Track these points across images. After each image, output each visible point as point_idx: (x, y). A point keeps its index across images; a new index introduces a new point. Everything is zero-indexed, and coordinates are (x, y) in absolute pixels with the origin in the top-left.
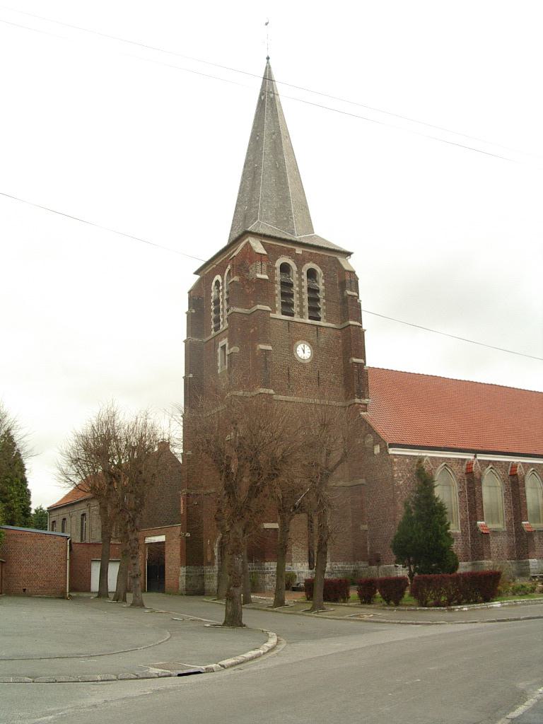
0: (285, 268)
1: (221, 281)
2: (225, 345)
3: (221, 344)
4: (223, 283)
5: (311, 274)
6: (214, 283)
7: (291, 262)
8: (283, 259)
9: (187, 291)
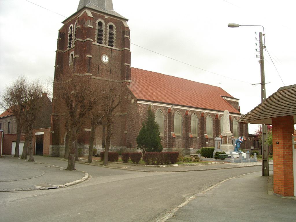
0: (100, 24)
1: (73, 27)
2: (73, 54)
3: (71, 53)
5: (111, 27)
6: (70, 28)
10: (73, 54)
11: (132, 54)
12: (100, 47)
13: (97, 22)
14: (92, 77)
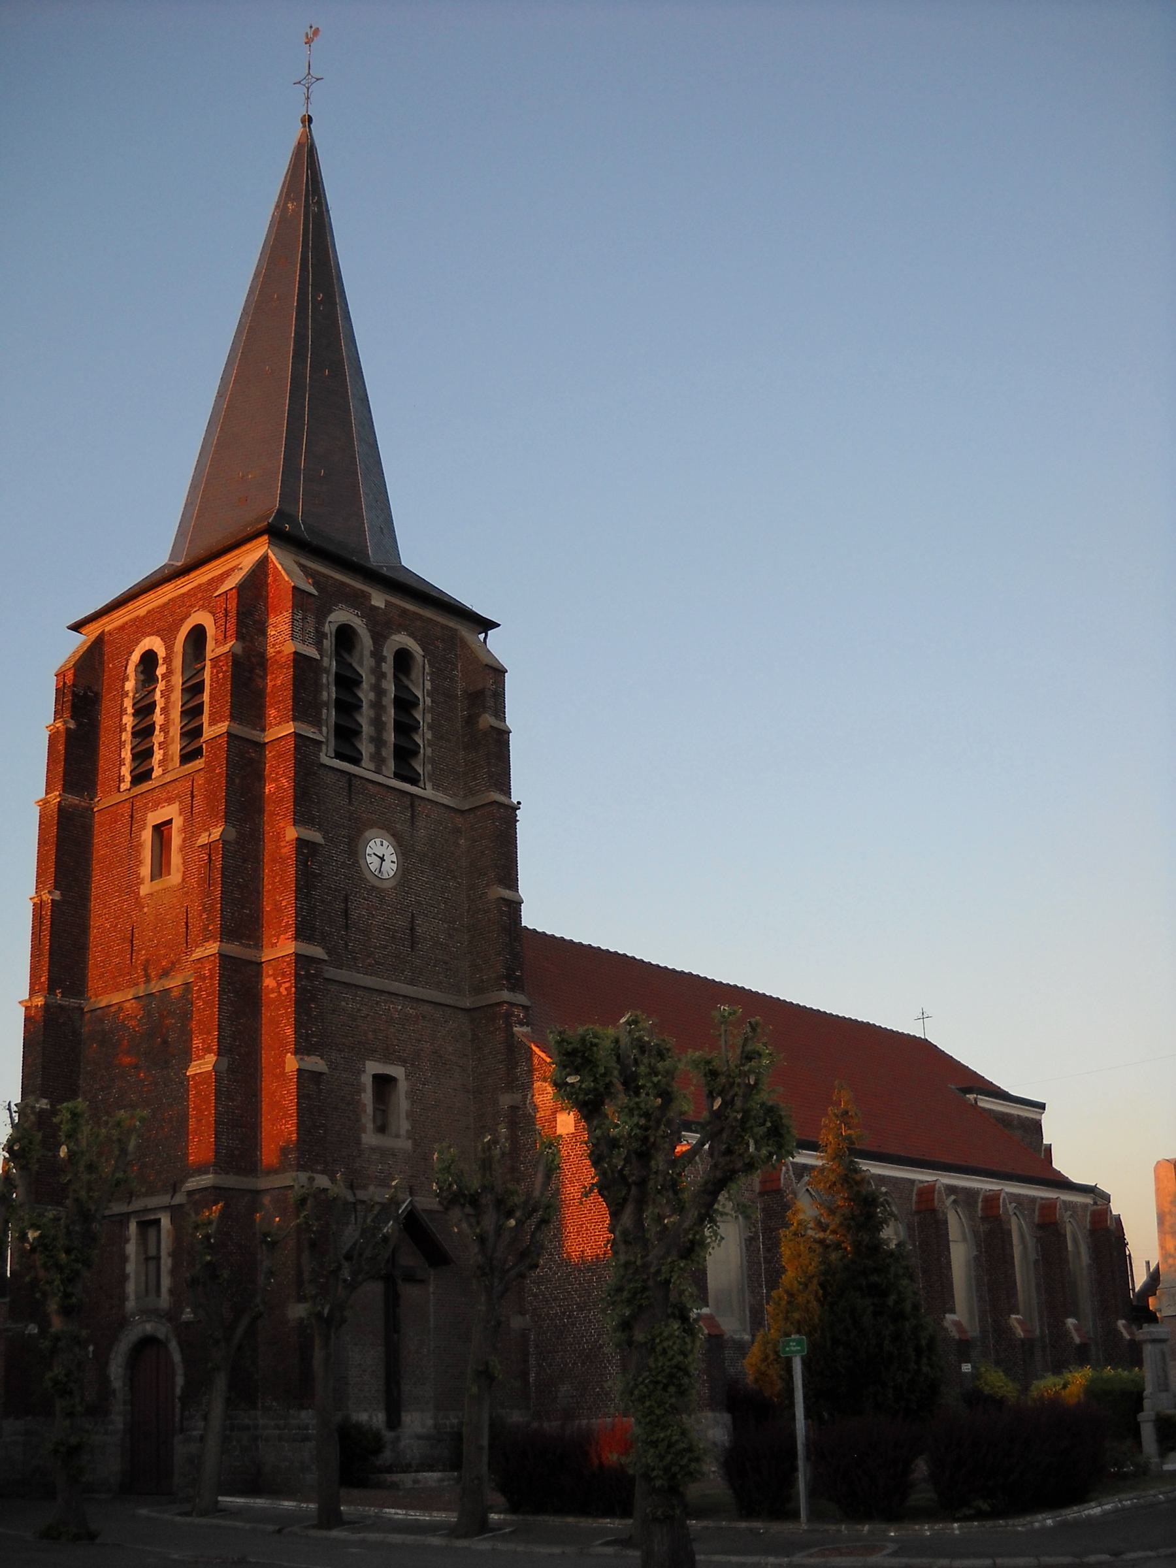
0: (345, 636)
1: (161, 653)
2: (170, 822)
3: (155, 817)
4: (168, 660)
5: (403, 659)
6: (135, 657)
7: (358, 623)
8: (341, 616)
9: (54, 671)
10: (170, 822)
12: (350, 781)
13: (329, 628)
14: (331, 972)
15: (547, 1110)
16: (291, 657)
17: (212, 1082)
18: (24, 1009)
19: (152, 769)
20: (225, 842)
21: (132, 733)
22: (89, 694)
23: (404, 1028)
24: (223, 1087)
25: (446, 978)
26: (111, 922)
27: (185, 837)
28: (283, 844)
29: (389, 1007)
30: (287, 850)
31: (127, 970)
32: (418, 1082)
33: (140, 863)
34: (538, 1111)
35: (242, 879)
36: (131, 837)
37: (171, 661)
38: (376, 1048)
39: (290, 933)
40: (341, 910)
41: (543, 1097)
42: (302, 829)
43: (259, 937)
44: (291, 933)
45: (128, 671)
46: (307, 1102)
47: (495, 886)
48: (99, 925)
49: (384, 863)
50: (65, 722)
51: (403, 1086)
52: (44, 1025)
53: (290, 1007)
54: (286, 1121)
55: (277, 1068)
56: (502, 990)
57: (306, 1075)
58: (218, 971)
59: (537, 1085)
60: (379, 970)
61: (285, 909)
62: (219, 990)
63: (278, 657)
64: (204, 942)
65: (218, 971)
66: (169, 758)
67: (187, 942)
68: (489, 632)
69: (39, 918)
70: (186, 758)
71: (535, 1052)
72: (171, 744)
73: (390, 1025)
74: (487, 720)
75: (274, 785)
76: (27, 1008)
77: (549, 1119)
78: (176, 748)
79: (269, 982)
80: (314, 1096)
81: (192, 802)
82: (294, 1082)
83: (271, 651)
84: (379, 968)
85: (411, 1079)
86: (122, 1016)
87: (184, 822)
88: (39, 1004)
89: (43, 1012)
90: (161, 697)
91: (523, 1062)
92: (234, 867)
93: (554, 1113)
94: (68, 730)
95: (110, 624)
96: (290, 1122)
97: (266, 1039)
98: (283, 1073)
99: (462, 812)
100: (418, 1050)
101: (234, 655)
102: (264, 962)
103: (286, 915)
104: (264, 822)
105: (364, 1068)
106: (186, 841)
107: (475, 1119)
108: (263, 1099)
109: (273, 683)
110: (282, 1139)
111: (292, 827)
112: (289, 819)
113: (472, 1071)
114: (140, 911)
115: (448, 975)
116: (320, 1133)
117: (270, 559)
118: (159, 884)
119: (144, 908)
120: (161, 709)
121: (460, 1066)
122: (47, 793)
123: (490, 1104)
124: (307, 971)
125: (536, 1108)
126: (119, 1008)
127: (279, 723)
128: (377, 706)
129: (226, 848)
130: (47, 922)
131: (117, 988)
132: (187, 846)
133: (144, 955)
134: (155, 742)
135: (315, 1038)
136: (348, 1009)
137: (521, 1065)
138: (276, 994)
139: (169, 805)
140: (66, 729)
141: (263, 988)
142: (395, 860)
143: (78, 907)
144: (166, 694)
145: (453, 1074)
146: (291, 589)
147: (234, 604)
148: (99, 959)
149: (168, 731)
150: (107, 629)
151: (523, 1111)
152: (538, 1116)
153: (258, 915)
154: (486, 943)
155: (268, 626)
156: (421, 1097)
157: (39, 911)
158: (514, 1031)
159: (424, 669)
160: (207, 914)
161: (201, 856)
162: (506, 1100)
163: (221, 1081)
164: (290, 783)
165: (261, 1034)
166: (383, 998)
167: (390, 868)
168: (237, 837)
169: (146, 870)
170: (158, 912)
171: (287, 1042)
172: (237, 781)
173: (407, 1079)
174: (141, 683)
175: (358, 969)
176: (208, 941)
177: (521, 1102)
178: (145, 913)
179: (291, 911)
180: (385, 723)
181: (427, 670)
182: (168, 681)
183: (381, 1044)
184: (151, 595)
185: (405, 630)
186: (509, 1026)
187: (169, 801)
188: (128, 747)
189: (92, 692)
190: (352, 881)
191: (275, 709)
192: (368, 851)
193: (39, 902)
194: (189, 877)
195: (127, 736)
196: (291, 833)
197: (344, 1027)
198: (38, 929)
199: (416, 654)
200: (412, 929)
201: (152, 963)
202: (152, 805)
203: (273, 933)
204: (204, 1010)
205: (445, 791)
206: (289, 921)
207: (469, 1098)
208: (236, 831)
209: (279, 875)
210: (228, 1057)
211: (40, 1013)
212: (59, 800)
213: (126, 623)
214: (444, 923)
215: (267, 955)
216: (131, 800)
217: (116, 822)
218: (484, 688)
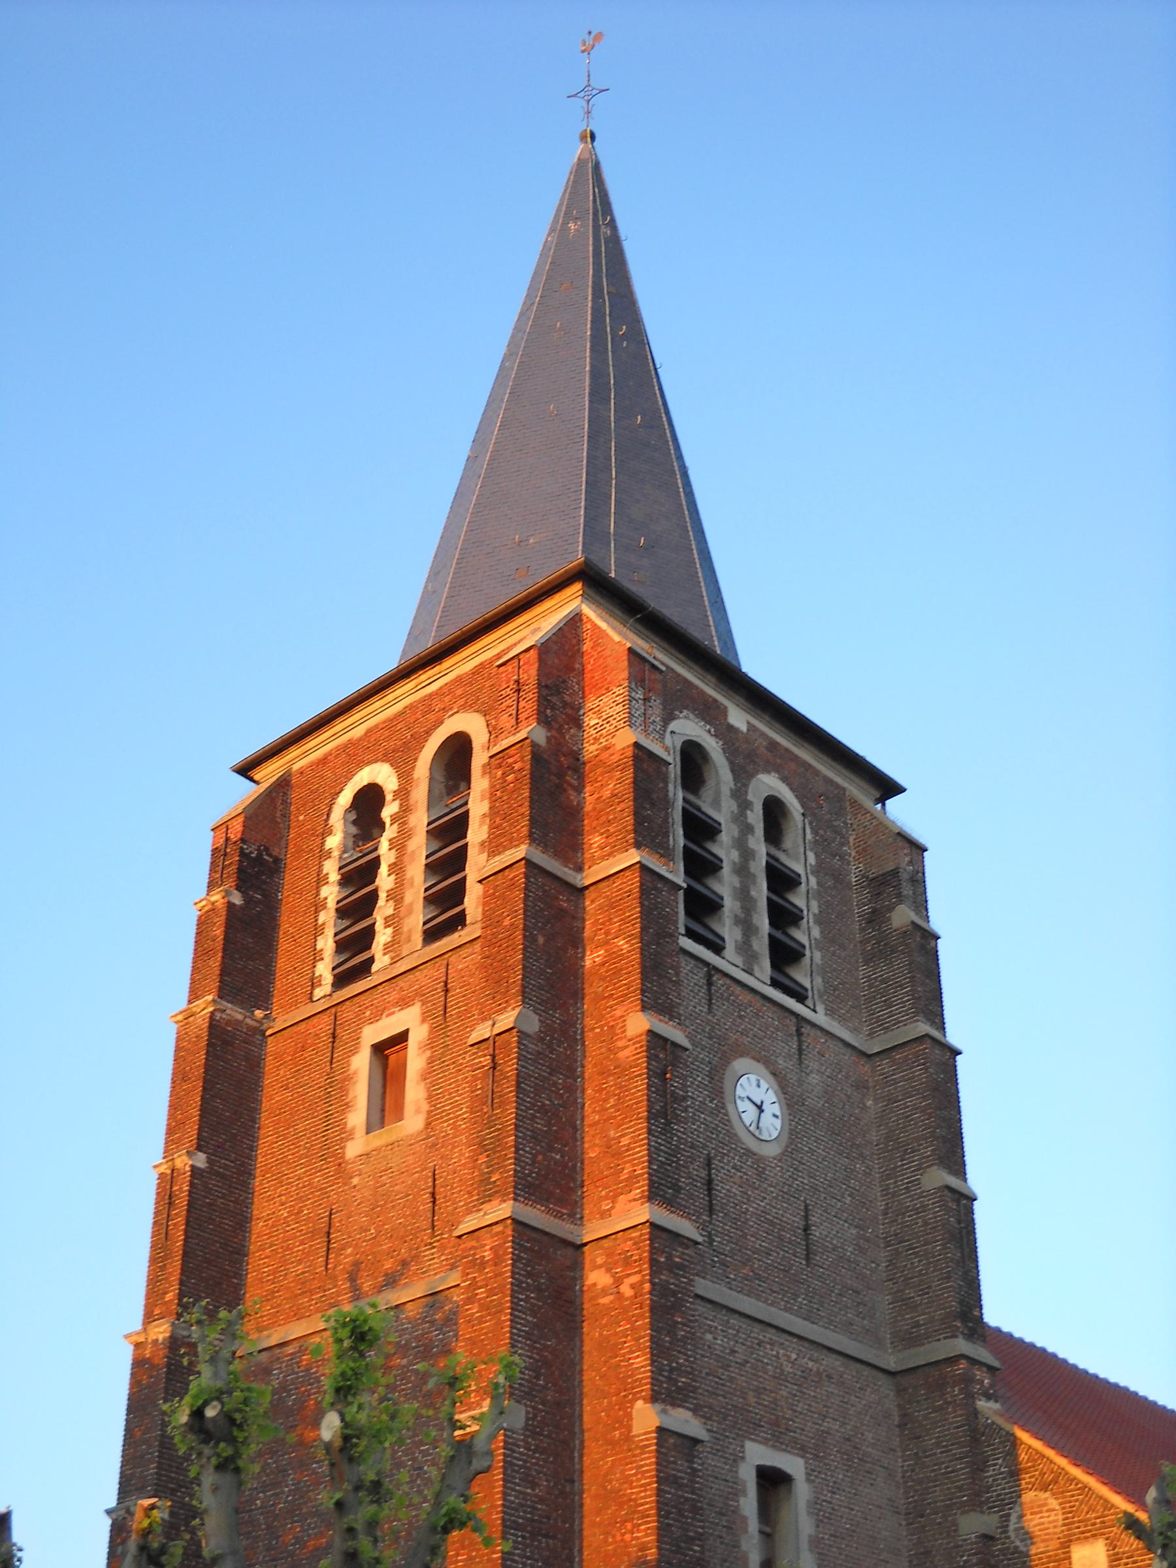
2: (402, 1038)
4: (403, 793)
5: (774, 810)
6: (345, 798)
9: (213, 823)
10: (402, 1038)
11: (944, 949)
15: (1052, 1539)
16: (630, 753)
17: (498, 1448)
18: (132, 1348)
19: (371, 960)
20: (522, 1035)
21: (337, 910)
22: (265, 857)
23: (801, 1392)
24: (515, 1458)
25: (858, 1316)
26: (291, 1206)
27: (431, 1057)
28: (620, 1044)
29: (778, 1353)
30: (631, 1053)
31: (316, 1284)
32: (825, 1487)
33: (347, 1106)
34: (1032, 1544)
35: (550, 1101)
36: (332, 1068)
37: (408, 793)
38: (760, 1420)
39: (638, 1191)
40: (703, 1181)
41: (1041, 1518)
42: (656, 1021)
43: (576, 1202)
44: (641, 1188)
45: (332, 821)
46: (673, 1491)
47: (935, 1168)
48: (268, 1215)
49: (762, 1115)
50: (227, 893)
51: (802, 1491)
52: (167, 1373)
53: (641, 1316)
54: (634, 1526)
55: (615, 1429)
56: (956, 1337)
57: (671, 1441)
58: (510, 1250)
59: (1028, 1497)
60: (761, 1289)
61: (627, 1150)
62: (512, 1284)
63: (605, 755)
64: (482, 1203)
65: (510, 1250)
66: (404, 937)
67: (433, 1227)
68: (888, 802)
69: (167, 1197)
70: (432, 934)
71: (1020, 1439)
72: (407, 916)
73: (781, 1385)
74: (902, 916)
75: (602, 952)
76: (138, 1345)
77: (1056, 1555)
78: (417, 919)
79: (597, 1278)
80: (685, 1481)
81: (446, 999)
82: (650, 1452)
83: (590, 749)
84: (760, 1286)
85: (813, 1481)
86: (306, 1360)
87: (430, 1032)
88: (161, 1337)
89: (167, 1350)
90: (390, 849)
91: (998, 1459)
92: (536, 1078)
93: (1066, 1545)
94: (230, 906)
95: (299, 759)
96: (643, 1527)
97: (592, 1377)
98: (628, 1438)
99: (869, 1056)
100: (822, 1431)
101: (534, 745)
102: (586, 1244)
103: (630, 1161)
104: (583, 1013)
105: (743, 1452)
106: (435, 1061)
107: (910, 1561)
108: (585, 1487)
109: (596, 796)
110: (626, 1558)
111: (640, 1013)
112: (632, 1002)
113: (903, 1477)
114: (345, 1184)
115: (861, 1313)
116: (695, 1551)
117: (584, 618)
118: (380, 1138)
119: (351, 1178)
120: (389, 866)
121: (884, 1468)
122: (190, 1002)
123: (940, 1534)
124: (669, 1258)
125: (1028, 1537)
126: (300, 1347)
127: (610, 855)
128: (742, 870)
129: (524, 1045)
130: (182, 1202)
131: (298, 1315)
132: (434, 1071)
133: (350, 1255)
134: (378, 918)
135: (684, 1377)
136: (716, 1347)
137: (995, 1465)
138: (611, 1297)
139: (402, 1009)
140: (229, 902)
141: (585, 1288)
142: (778, 1113)
143: (234, 1185)
144: (399, 845)
145: (875, 1480)
146: (626, 652)
147: (533, 672)
148: (266, 1270)
149: (402, 898)
150: (296, 767)
151: (1003, 1544)
152: (1033, 1552)
153: (575, 1166)
154: (920, 1261)
155: (584, 714)
156: (830, 1513)
157: (168, 1187)
158: (977, 1407)
159: (805, 834)
160: (488, 1156)
161: (476, 1061)
162: (973, 1524)
163: (514, 1448)
164: (633, 944)
165: (582, 1370)
166: (768, 1335)
167: (772, 1124)
168: (540, 1031)
169: (357, 1118)
170: (378, 1182)
171: (636, 1381)
172: (541, 940)
173: (808, 1480)
174: (352, 839)
175: (729, 1283)
176: (490, 1201)
177: (997, 1528)
178: (355, 1187)
179: (640, 1152)
180: (756, 901)
181: (809, 836)
182: (405, 823)
183: (768, 1415)
184: (376, 704)
185: (777, 771)
186: (971, 1397)
187: (404, 1003)
188: (330, 932)
189: (270, 855)
190: (717, 1136)
191: (602, 834)
192: (739, 1091)
193: (169, 1172)
194: (438, 1119)
195: (327, 917)
196: (638, 1023)
197: (711, 1378)
198: (165, 1216)
199: (791, 808)
200: (806, 1229)
201: (366, 1266)
202: (371, 1014)
203: (603, 1193)
204: (481, 1320)
205: (842, 1020)
206: (635, 1171)
207: (900, 1525)
208: (540, 1020)
209: (615, 1095)
210: (526, 1405)
211: (161, 1353)
212: (211, 1009)
213: (330, 753)
214: (852, 1228)
215: (592, 1230)
216: (333, 1010)
217: (304, 1049)
218: (897, 868)
